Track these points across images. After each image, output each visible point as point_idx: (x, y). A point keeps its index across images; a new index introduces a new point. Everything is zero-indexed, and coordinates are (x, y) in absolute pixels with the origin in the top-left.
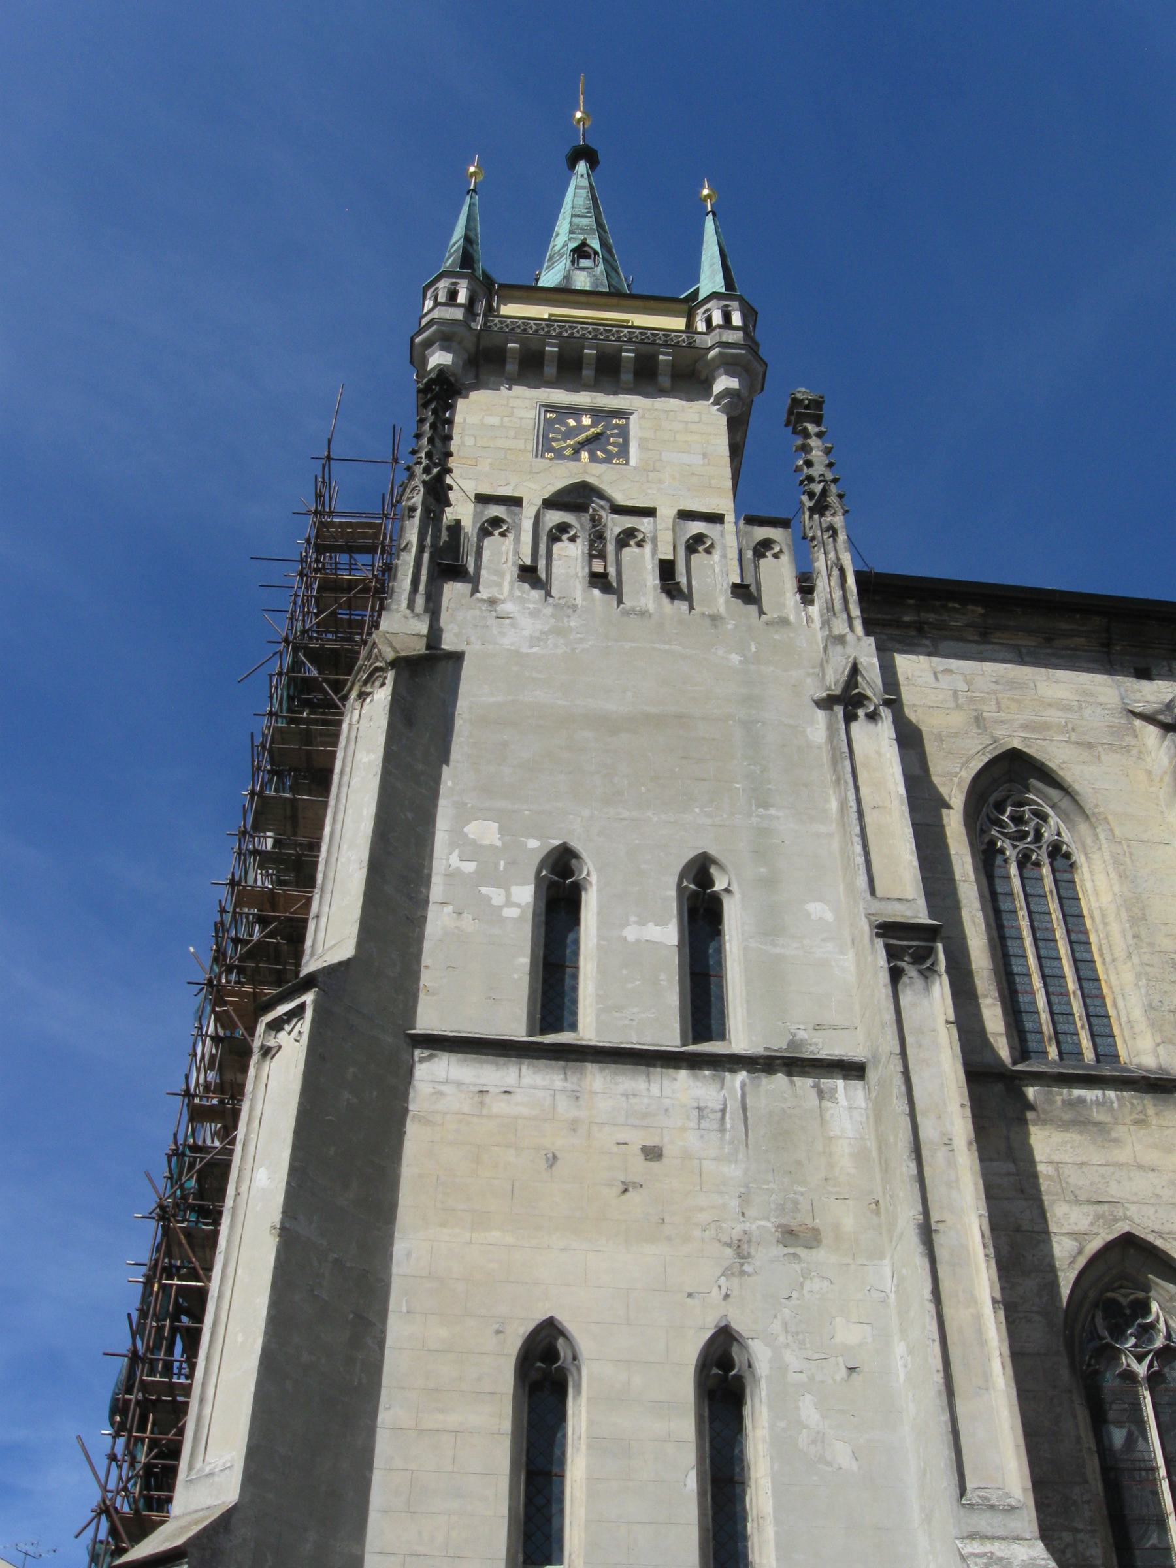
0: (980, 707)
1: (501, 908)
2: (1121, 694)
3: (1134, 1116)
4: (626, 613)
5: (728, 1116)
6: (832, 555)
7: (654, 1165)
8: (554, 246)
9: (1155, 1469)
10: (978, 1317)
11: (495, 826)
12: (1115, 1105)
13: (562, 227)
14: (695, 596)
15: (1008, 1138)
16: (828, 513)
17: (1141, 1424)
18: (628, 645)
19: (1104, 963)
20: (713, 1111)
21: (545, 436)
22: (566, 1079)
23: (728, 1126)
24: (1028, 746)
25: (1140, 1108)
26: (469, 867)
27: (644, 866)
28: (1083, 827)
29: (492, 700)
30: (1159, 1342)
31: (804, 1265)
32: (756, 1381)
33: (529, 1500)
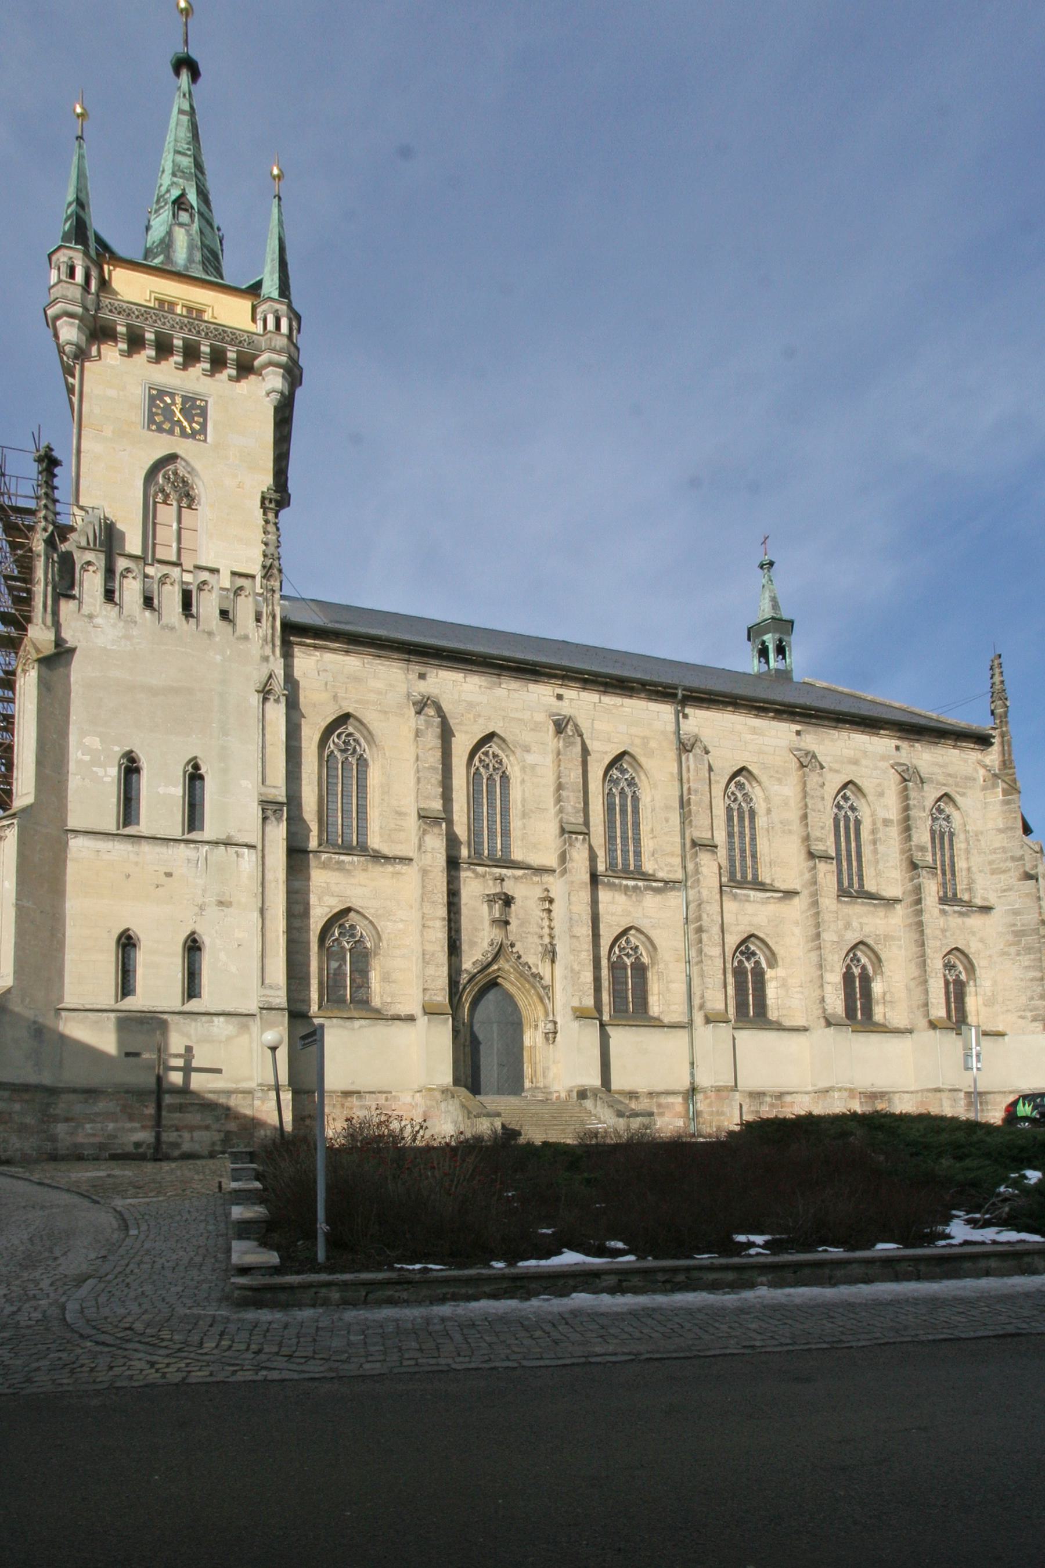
4: (164, 628)
6: (270, 607)
8: (161, 185)
10: (278, 937)
13: (170, 138)
14: (201, 619)
16: (272, 579)
21: (150, 410)
26: (87, 758)
28: (375, 749)
29: (94, 675)
33: (726, 704)
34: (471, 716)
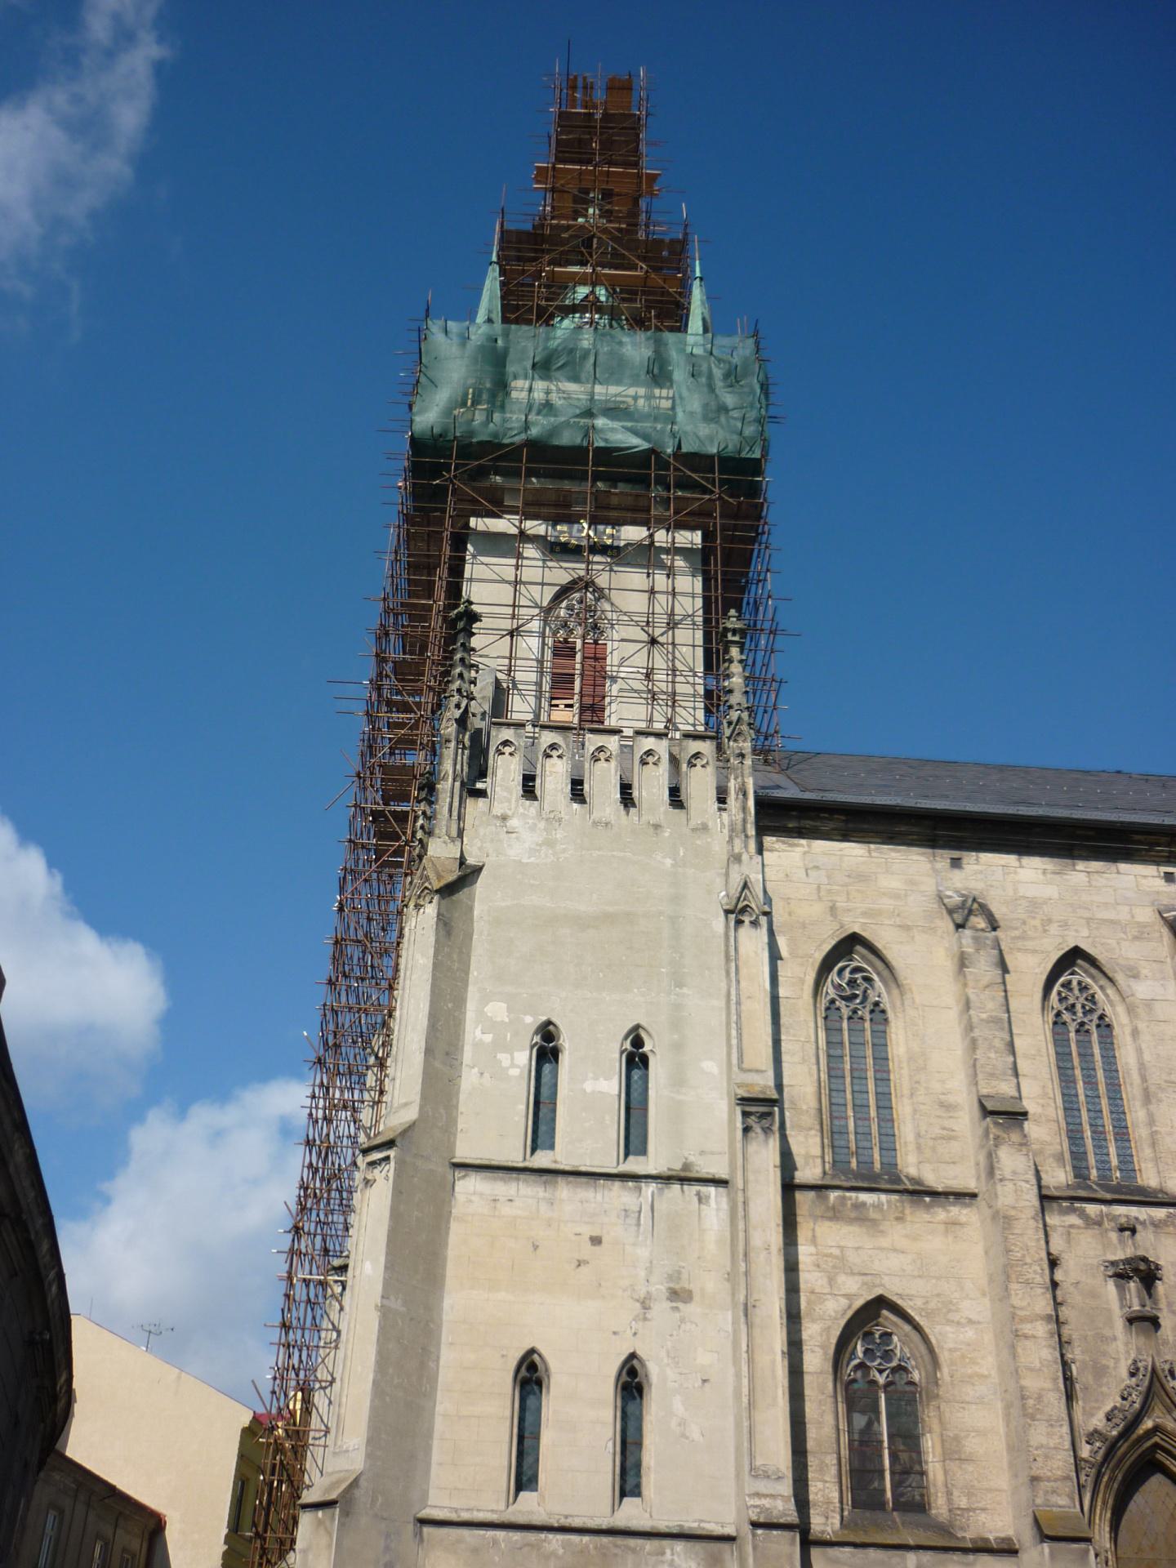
0: (835, 898)
1: (508, 1068)
2: (937, 883)
3: (897, 1215)
5: (642, 1215)
7: (597, 1248)
9: (881, 1442)
10: (773, 1362)
11: (504, 1005)
12: (885, 1207)
15: (813, 1230)
17: (877, 1413)
18: (596, 853)
19: (896, 1096)
20: (633, 1212)
22: (545, 1191)
23: (642, 1222)
24: (864, 930)
25: (901, 1209)
27: (599, 1035)
28: (895, 992)
29: (503, 904)
30: (894, 1364)
31: (682, 1314)
32: (650, 1386)
34: (1037, 923)
